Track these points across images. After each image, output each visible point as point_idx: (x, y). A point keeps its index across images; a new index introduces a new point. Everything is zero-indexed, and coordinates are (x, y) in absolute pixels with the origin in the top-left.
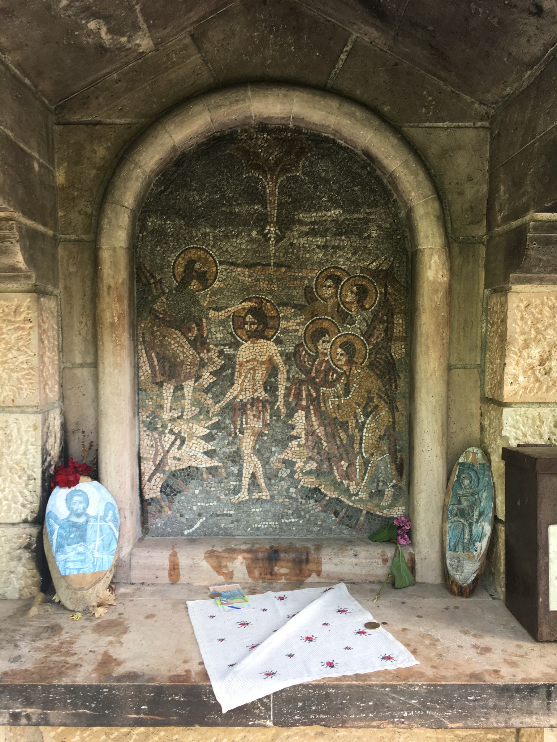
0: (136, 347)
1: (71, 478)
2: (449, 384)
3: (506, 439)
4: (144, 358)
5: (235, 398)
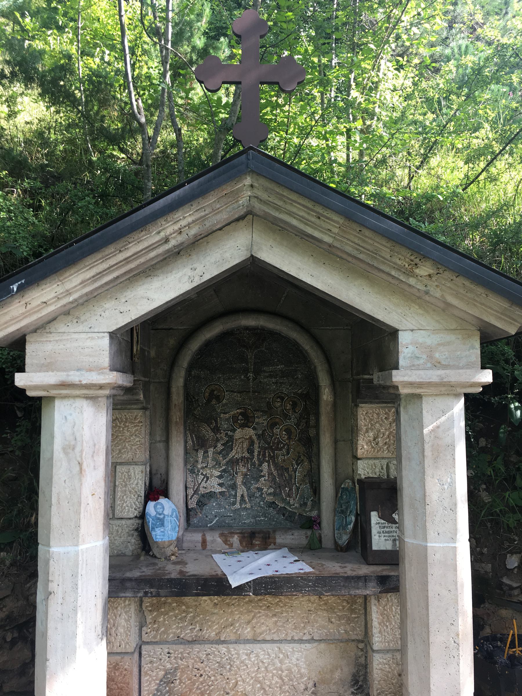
0: (185, 432)
1: (156, 496)
2: (336, 449)
3: (360, 475)
4: (189, 437)
5: (233, 457)
